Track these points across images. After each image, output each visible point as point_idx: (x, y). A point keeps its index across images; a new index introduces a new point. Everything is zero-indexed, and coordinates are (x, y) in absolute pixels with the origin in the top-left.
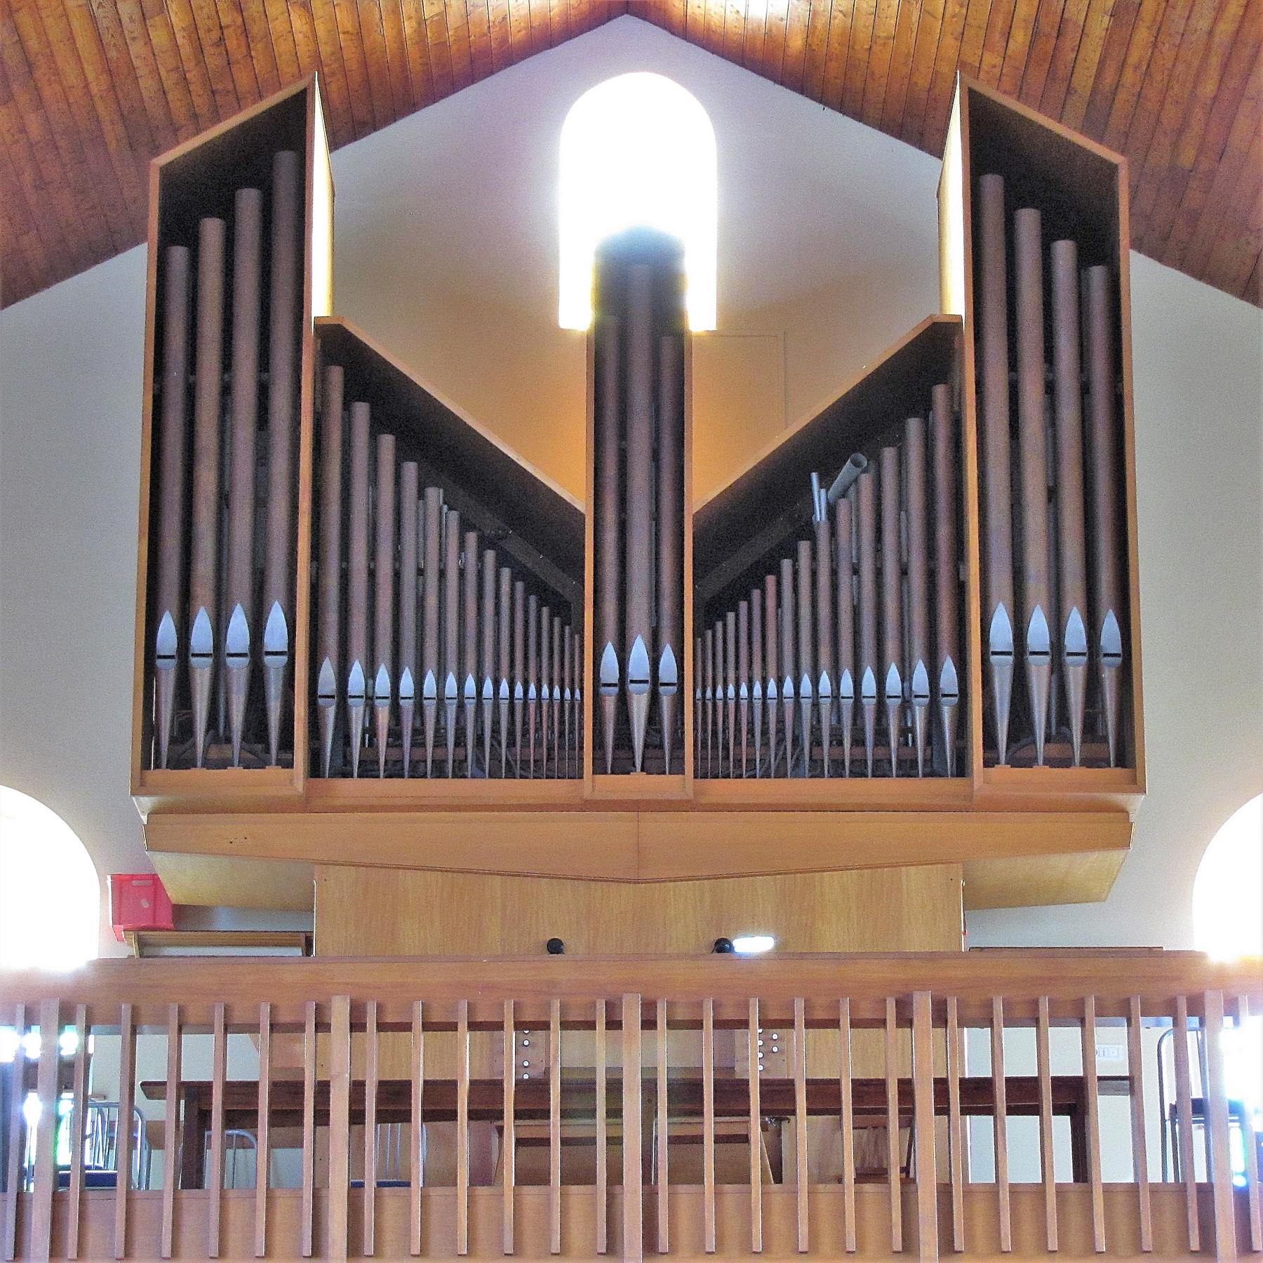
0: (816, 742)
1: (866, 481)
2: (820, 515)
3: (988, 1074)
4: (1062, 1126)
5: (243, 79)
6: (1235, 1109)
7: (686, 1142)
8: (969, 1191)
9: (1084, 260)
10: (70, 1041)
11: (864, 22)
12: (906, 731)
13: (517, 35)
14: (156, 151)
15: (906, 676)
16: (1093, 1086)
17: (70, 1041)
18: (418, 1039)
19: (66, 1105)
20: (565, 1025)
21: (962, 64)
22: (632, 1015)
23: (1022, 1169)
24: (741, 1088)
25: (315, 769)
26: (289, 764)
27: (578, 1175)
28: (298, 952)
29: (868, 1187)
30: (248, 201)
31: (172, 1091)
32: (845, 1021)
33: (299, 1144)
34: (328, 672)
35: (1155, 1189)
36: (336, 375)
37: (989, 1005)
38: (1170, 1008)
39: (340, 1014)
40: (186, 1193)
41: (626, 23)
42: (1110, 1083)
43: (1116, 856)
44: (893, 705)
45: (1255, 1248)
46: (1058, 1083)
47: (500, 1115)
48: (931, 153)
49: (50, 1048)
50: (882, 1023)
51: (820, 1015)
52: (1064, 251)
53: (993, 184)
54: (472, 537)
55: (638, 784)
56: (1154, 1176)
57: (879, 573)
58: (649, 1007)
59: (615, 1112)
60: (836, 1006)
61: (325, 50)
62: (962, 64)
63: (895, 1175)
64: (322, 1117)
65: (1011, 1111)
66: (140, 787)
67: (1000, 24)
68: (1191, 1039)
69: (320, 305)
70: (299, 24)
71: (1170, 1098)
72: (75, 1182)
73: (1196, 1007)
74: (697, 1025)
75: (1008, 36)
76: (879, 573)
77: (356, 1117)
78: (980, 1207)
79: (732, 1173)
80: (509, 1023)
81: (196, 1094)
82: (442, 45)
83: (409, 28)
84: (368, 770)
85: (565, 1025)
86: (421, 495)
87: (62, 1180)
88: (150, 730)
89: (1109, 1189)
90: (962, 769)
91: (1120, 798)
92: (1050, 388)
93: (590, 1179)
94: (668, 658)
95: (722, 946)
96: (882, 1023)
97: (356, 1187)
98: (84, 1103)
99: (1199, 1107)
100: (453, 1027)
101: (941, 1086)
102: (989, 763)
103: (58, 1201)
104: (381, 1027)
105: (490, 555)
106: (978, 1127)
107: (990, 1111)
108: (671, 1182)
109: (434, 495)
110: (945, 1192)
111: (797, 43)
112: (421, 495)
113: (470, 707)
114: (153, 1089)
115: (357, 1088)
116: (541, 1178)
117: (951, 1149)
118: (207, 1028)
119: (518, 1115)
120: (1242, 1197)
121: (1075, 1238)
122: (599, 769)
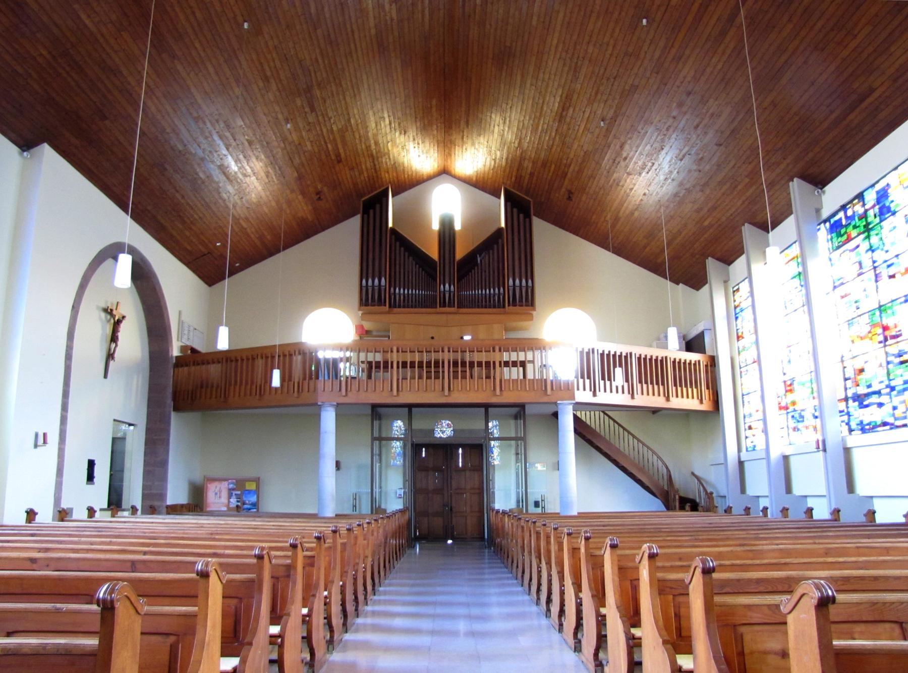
0: (478, 302)
1: (487, 257)
2: (479, 261)
3: (516, 360)
4: (521, 369)
5: (377, 185)
6: (550, 366)
7: (455, 372)
8: (505, 380)
9: (525, 218)
10: (348, 354)
11: (486, 175)
12: (494, 300)
13: (425, 178)
14: (362, 197)
15: (494, 290)
16: (527, 362)
17: (348, 354)
18: (409, 354)
19: (348, 364)
20: (434, 352)
21: (503, 183)
22: (446, 350)
23: (514, 377)
24: (465, 363)
25: (390, 306)
26: (385, 305)
27: (437, 377)
28: (387, 339)
29: (487, 380)
30: (378, 206)
31: (366, 362)
32: (483, 351)
33: (388, 372)
34: (392, 289)
35: (537, 380)
36: (393, 237)
37: (508, 348)
38: (540, 349)
39: (395, 350)
40: (369, 380)
41: (444, 175)
42: (530, 362)
43: (531, 322)
44: (492, 295)
45: (548, 394)
46: (513, 362)
47: (423, 367)
48: (496, 197)
49: (345, 355)
50: (490, 351)
51: (479, 350)
52: (521, 216)
53: (509, 204)
54: (417, 266)
55: (447, 309)
56: (537, 378)
57: (489, 272)
58: (449, 349)
59: (443, 367)
60: (482, 348)
61: (391, 180)
62: (503, 183)
63: (492, 377)
64: (392, 367)
65: (512, 366)
66: (359, 310)
67: (510, 176)
68: (544, 354)
69: (390, 225)
70: (387, 175)
71: (540, 364)
72: (349, 378)
73: (544, 348)
74: (457, 352)
75: (511, 178)
76: (489, 272)
77: (398, 367)
78: (507, 383)
79: (464, 377)
80: (424, 351)
81: (370, 363)
82: (412, 179)
83: (406, 176)
84: (400, 307)
85: (434, 352)
86: (408, 258)
87: (347, 378)
88: (361, 300)
89: (529, 380)
90: (504, 307)
91: (531, 312)
92: (519, 240)
93: (439, 378)
94: (452, 287)
95: (462, 338)
96: (490, 351)
97: (398, 380)
98: (351, 365)
99: (545, 366)
100: (415, 352)
101: (500, 362)
102: (509, 305)
103: (347, 382)
104: (402, 352)
105: (421, 269)
106: (506, 370)
107: (509, 366)
108: (453, 378)
109: (411, 258)
110: (501, 381)
111: (474, 179)
112: (408, 258)
113: (417, 296)
114: (363, 362)
115: (398, 363)
116: (431, 378)
117: (502, 373)
118: (372, 352)
119: (426, 367)
120: (552, 382)
121: (523, 388)
122: (440, 307)
